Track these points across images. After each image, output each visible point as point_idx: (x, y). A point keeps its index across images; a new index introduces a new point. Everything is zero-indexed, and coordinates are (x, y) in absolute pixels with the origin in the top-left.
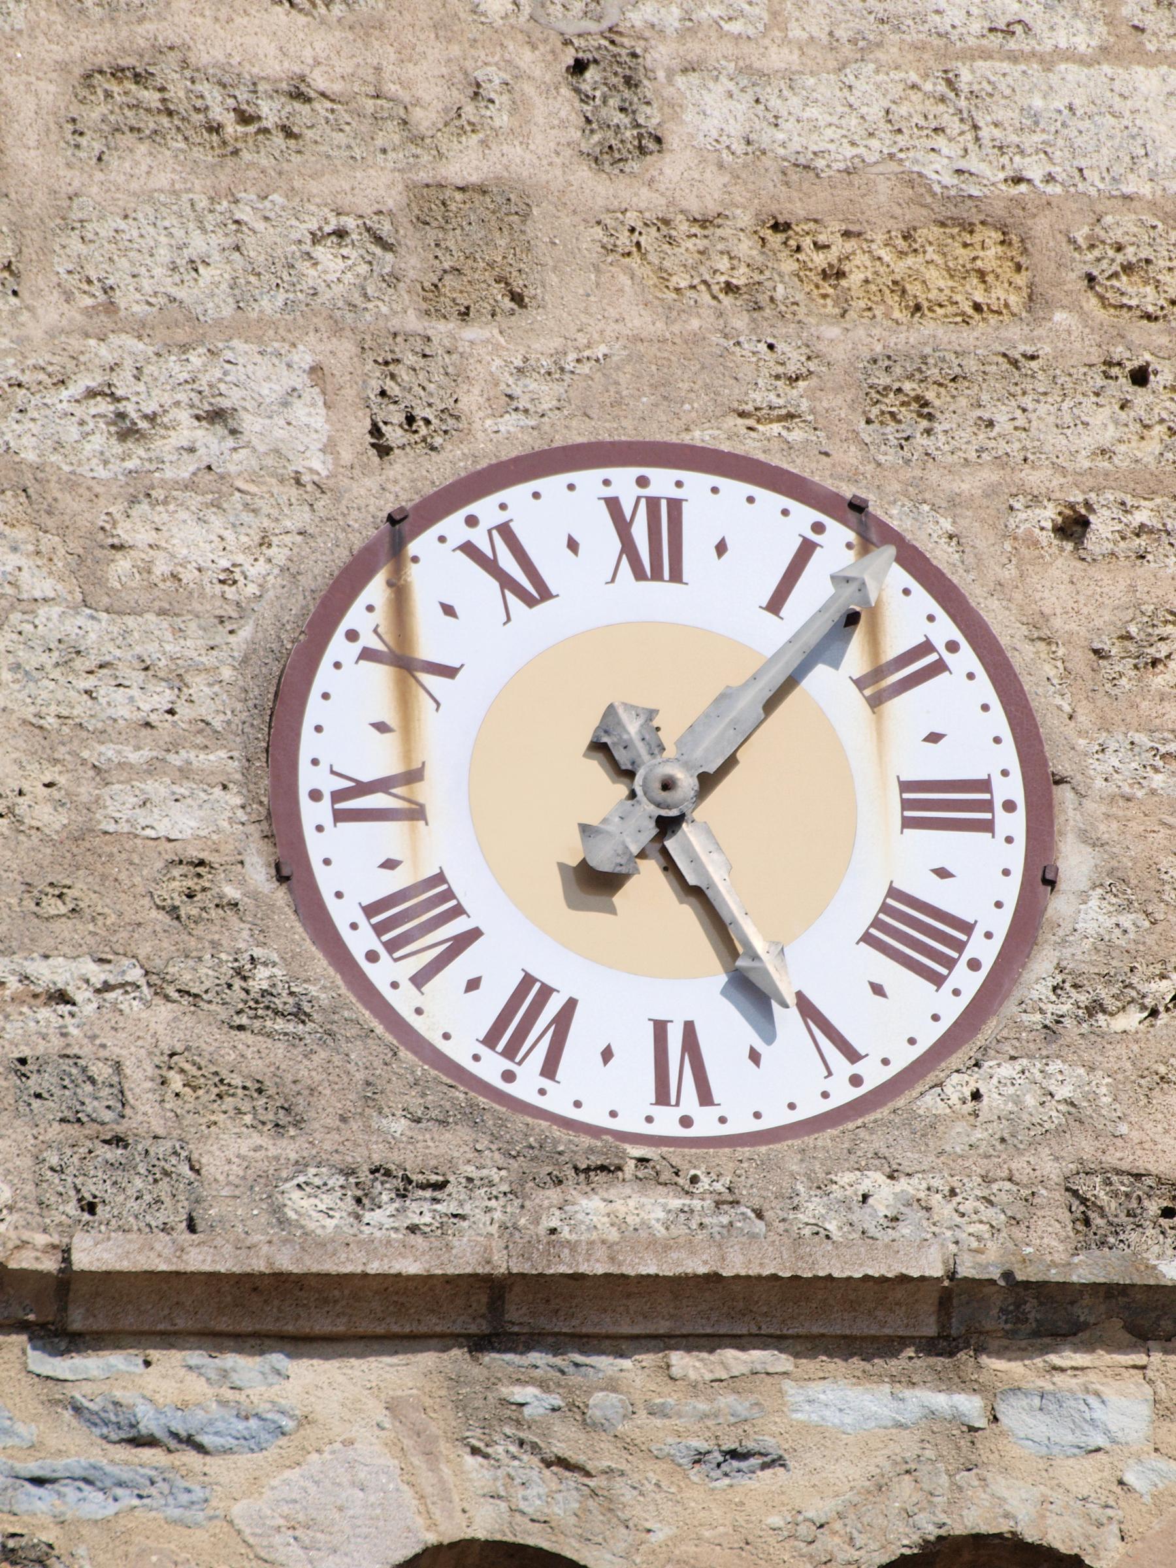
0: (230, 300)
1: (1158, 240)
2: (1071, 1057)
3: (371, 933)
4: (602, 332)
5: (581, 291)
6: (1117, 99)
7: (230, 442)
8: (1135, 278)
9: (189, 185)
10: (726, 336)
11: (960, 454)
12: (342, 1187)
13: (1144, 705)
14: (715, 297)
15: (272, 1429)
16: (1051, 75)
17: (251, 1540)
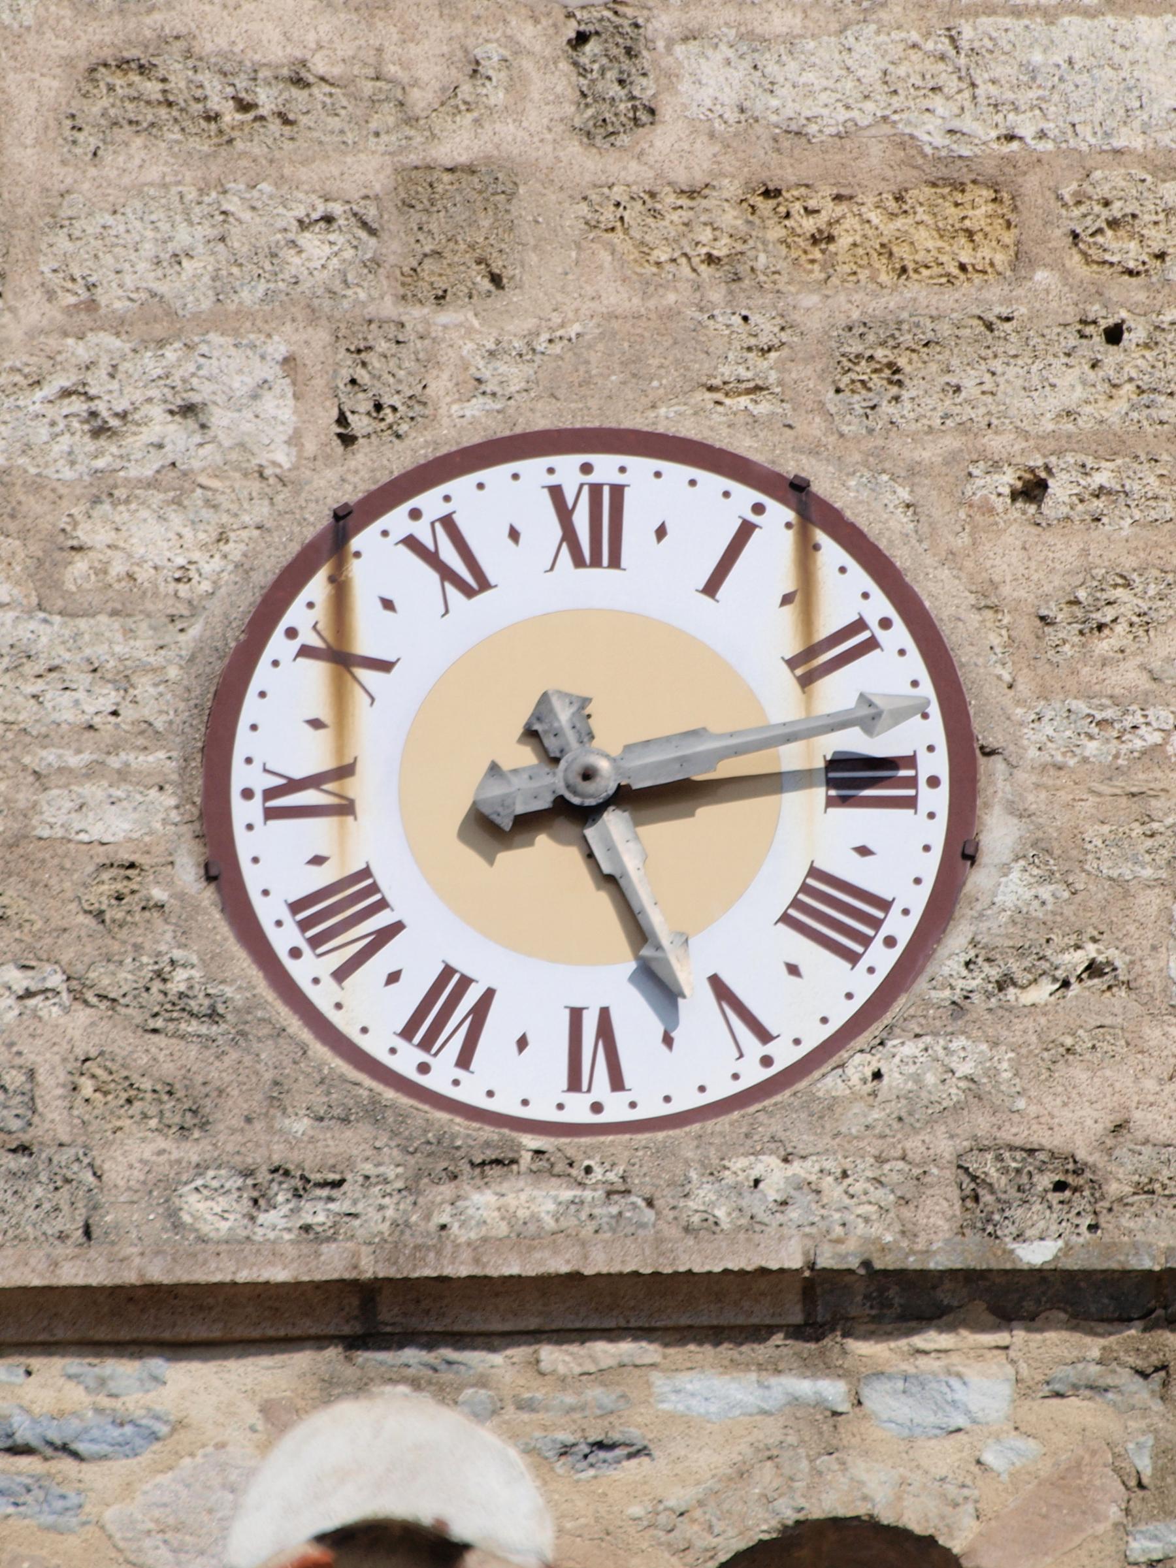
0: (211, 293)
1: (1146, 194)
2: (975, 1033)
3: (296, 930)
4: (577, 310)
5: (560, 270)
6: (1118, 50)
7: (197, 438)
8: (1121, 233)
9: (180, 177)
10: (701, 310)
11: (925, 421)
12: (239, 1189)
13: (1085, 671)
14: (694, 270)
15: (144, 1434)
16: (1053, 28)
17: (121, 1544)
